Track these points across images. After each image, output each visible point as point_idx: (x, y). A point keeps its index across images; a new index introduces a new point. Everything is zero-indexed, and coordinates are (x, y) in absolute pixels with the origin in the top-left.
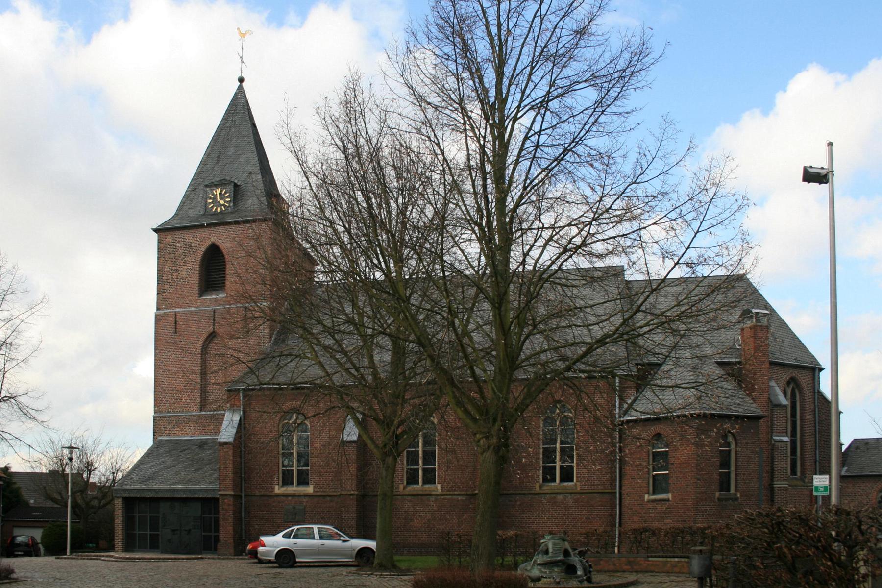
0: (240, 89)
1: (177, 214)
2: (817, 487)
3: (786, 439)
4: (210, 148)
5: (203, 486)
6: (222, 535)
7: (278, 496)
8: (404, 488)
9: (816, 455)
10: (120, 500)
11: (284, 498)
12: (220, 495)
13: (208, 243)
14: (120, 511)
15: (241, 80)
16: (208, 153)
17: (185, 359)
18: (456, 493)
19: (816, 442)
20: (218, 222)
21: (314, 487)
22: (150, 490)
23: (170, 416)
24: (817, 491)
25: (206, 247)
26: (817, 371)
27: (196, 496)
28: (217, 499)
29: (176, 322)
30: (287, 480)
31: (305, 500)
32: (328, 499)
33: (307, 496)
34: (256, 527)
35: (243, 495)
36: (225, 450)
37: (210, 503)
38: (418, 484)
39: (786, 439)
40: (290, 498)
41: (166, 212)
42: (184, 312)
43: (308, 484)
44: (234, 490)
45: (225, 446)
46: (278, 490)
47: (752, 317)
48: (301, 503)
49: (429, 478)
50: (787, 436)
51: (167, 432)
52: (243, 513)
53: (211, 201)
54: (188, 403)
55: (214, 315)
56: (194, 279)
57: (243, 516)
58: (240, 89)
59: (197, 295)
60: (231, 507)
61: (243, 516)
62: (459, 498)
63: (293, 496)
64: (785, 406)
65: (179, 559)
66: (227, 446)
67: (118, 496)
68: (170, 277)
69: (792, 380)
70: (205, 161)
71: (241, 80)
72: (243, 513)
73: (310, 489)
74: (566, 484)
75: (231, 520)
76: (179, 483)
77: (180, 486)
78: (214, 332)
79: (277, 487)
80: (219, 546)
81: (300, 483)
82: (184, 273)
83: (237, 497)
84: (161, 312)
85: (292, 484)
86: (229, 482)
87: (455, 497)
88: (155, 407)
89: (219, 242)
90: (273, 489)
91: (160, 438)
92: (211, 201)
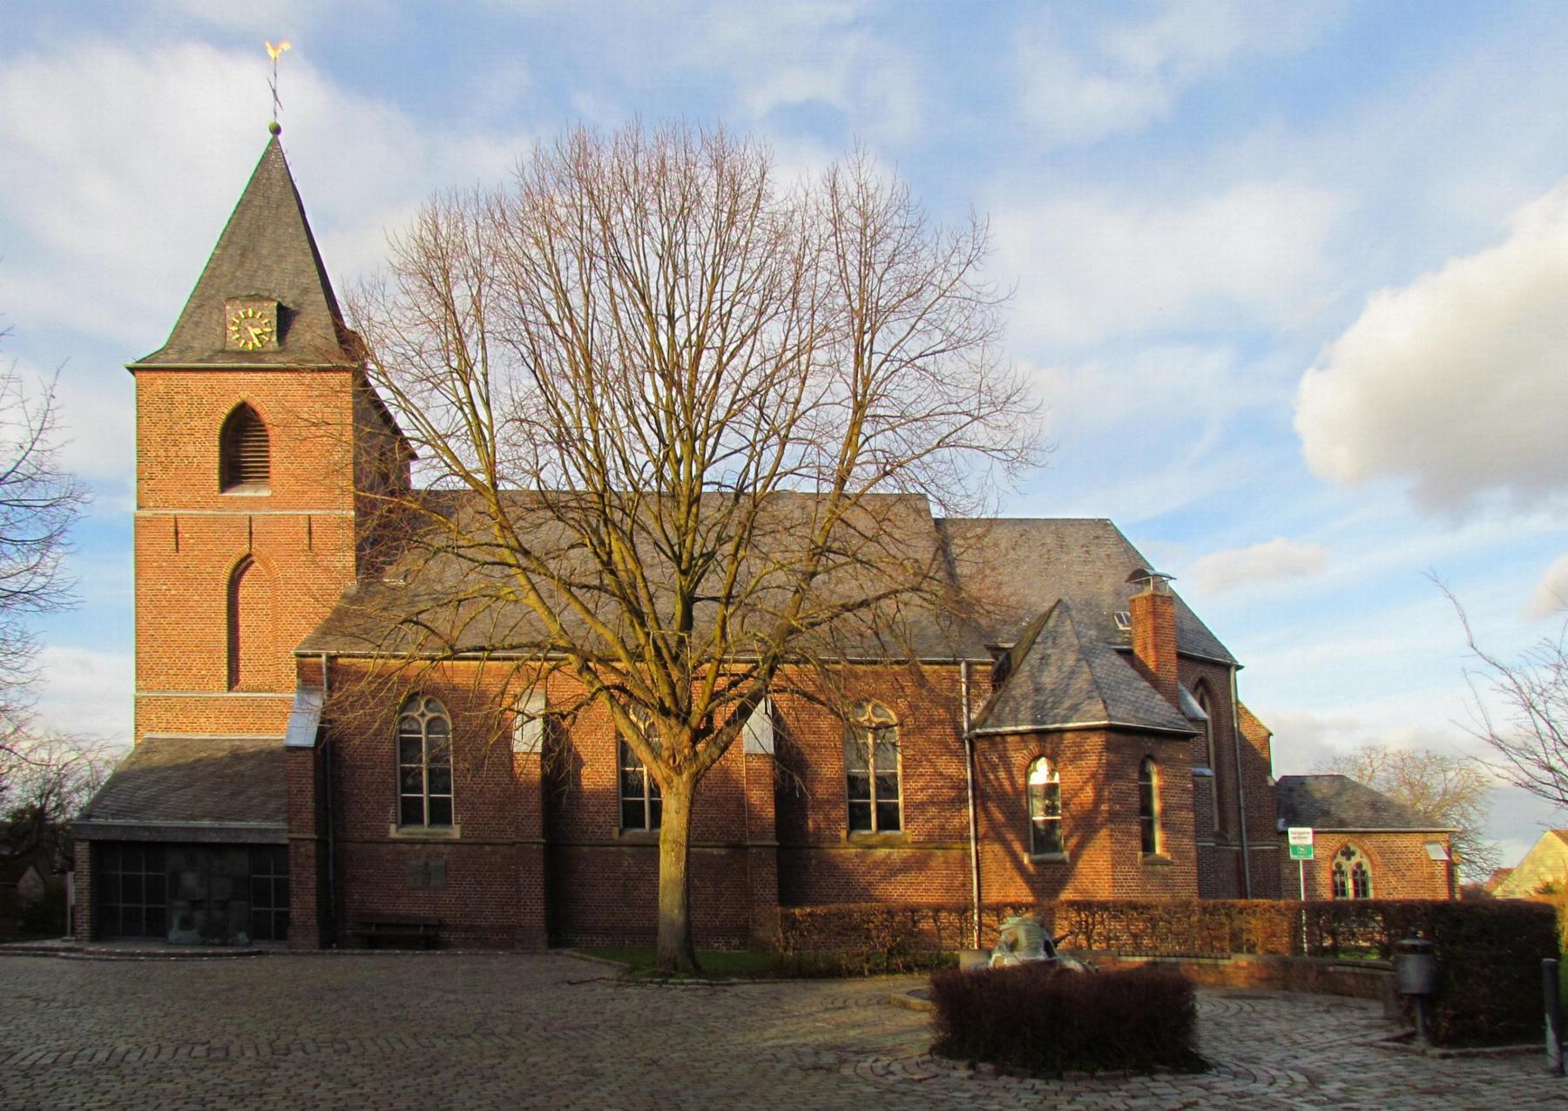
0: (274, 143)
1: (170, 345)
2: (1295, 847)
3: (1208, 772)
4: (225, 238)
5: (253, 824)
6: (295, 913)
7: (395, 842)
8: (621, 833)
9: (1239, 798)
10: (86, 845)
11: (406, 847)
12: (292, 839)
13: (234, 402)
14: (86, 866)
15: (276, 130)
16: (228, 240)
17: (196, 598)
18: (709, 843)
19: (1237, 778)
20: (250, 361)
21: (462, 829)
22: (148, 829)
23: (168, 698)
24: (1296, 853)
25: (230, 408)
26: (1233, 670)
27: (241, 841)
28: (286, 846)
29: (177, 533)
30: (410, 814)
31: (448, 849)
32: (487, 848)
33: (447, 843)
34: (356, 897)
35: (330, 840)
36: (299, 760)
37: (264, 853)
38: (643, 826)
39: (1208, 772)
40: (418, 847)
41: (153, 338)
42: (191, 517)
43: (449, 822)
44: (544, 836)
45: (299, 753)
46: (394, 832)
47: (1148, 582)
48: (439, 855)
49: (441, 814)
50: (1209, 767)
51: (164, 725)
52: (331, 872)
53: (234, 328)
54: (203, 677)
55: (251, 527)
56: (210, 457)
57: (331, 877)
58: (274, 143)
59: (216, 488)
60: (313, 862)
61: (331, 877)
62: (715, 851)
63: (425, 842)
64: (1204, 721)
65: (221, 955)
66: (303, 753)
67: (82, 837)
68: (162, 453)
69: (1202, 682)
70: (218, 259)
71: (276, 130)
72: (331, 872)
73: (455, 832)
74: (888, 833)
75: (312, 884)
76: (203, 817)
77: (206, 823)
78: (249, 556)
79: (393, 827)
80: (291, 932)
81: (433, 822)
82: (190, 448)
83: (322, 843)
84: (146, 513)
85: (421, 821)
86: (308, 816)
87: (708, 850)
88: (137, 678)
89: (256, 402)
90: (387, 831)
91: (148, 735)
92: (234, 328)
